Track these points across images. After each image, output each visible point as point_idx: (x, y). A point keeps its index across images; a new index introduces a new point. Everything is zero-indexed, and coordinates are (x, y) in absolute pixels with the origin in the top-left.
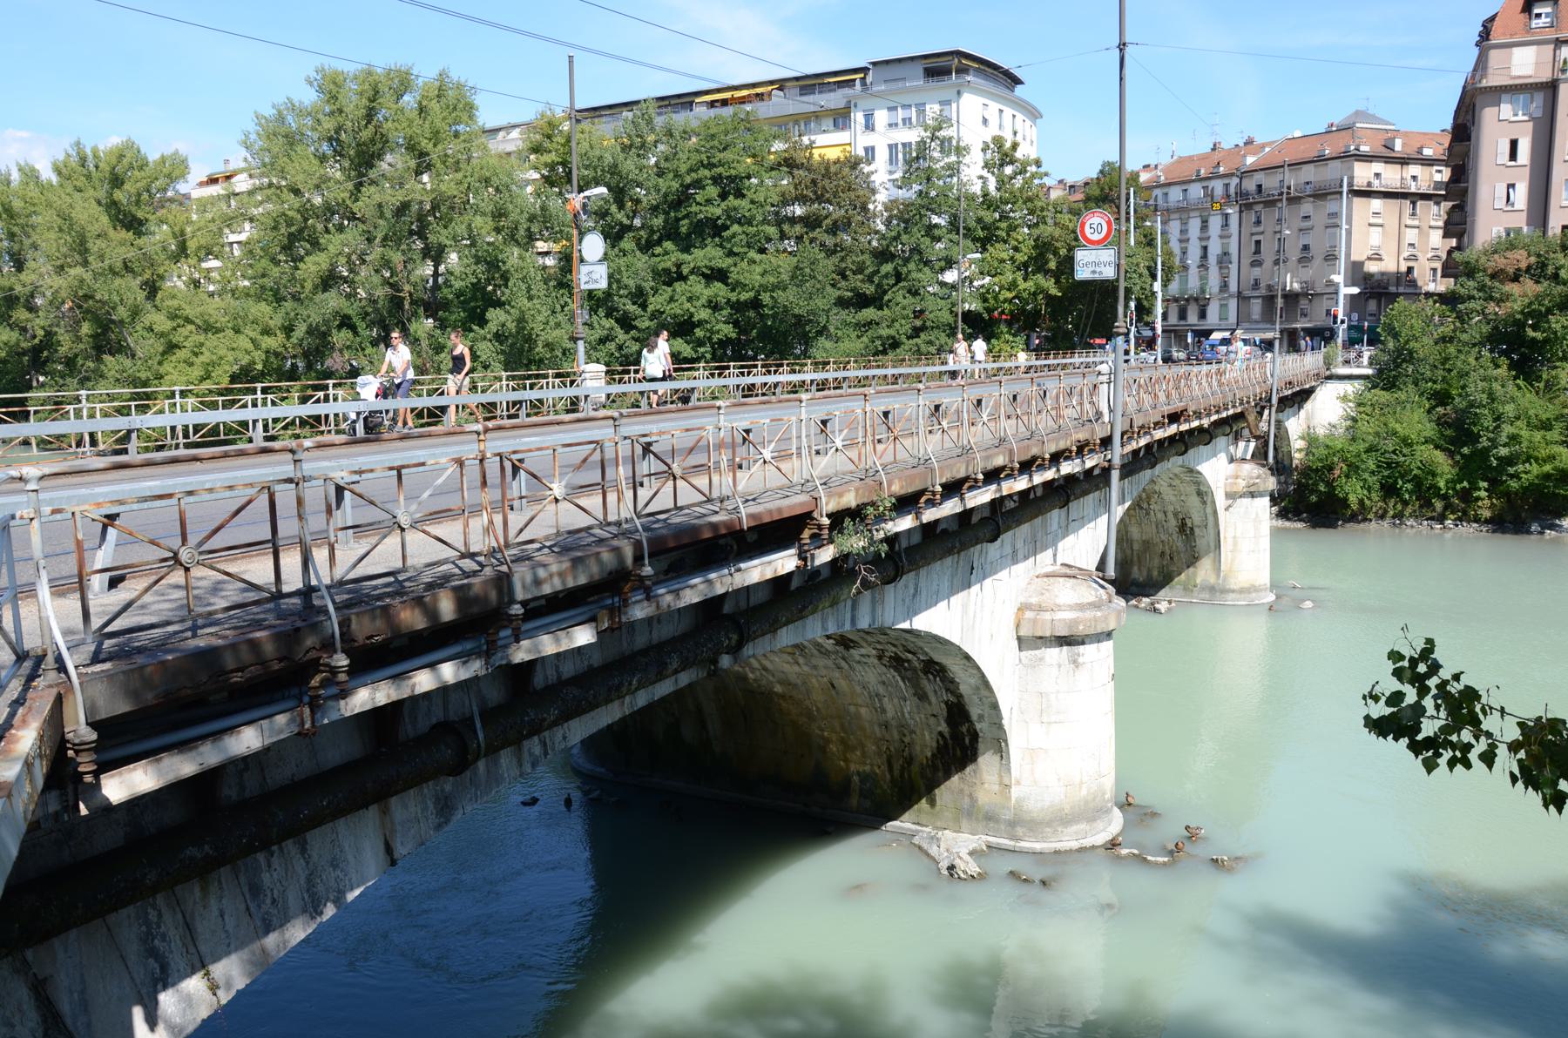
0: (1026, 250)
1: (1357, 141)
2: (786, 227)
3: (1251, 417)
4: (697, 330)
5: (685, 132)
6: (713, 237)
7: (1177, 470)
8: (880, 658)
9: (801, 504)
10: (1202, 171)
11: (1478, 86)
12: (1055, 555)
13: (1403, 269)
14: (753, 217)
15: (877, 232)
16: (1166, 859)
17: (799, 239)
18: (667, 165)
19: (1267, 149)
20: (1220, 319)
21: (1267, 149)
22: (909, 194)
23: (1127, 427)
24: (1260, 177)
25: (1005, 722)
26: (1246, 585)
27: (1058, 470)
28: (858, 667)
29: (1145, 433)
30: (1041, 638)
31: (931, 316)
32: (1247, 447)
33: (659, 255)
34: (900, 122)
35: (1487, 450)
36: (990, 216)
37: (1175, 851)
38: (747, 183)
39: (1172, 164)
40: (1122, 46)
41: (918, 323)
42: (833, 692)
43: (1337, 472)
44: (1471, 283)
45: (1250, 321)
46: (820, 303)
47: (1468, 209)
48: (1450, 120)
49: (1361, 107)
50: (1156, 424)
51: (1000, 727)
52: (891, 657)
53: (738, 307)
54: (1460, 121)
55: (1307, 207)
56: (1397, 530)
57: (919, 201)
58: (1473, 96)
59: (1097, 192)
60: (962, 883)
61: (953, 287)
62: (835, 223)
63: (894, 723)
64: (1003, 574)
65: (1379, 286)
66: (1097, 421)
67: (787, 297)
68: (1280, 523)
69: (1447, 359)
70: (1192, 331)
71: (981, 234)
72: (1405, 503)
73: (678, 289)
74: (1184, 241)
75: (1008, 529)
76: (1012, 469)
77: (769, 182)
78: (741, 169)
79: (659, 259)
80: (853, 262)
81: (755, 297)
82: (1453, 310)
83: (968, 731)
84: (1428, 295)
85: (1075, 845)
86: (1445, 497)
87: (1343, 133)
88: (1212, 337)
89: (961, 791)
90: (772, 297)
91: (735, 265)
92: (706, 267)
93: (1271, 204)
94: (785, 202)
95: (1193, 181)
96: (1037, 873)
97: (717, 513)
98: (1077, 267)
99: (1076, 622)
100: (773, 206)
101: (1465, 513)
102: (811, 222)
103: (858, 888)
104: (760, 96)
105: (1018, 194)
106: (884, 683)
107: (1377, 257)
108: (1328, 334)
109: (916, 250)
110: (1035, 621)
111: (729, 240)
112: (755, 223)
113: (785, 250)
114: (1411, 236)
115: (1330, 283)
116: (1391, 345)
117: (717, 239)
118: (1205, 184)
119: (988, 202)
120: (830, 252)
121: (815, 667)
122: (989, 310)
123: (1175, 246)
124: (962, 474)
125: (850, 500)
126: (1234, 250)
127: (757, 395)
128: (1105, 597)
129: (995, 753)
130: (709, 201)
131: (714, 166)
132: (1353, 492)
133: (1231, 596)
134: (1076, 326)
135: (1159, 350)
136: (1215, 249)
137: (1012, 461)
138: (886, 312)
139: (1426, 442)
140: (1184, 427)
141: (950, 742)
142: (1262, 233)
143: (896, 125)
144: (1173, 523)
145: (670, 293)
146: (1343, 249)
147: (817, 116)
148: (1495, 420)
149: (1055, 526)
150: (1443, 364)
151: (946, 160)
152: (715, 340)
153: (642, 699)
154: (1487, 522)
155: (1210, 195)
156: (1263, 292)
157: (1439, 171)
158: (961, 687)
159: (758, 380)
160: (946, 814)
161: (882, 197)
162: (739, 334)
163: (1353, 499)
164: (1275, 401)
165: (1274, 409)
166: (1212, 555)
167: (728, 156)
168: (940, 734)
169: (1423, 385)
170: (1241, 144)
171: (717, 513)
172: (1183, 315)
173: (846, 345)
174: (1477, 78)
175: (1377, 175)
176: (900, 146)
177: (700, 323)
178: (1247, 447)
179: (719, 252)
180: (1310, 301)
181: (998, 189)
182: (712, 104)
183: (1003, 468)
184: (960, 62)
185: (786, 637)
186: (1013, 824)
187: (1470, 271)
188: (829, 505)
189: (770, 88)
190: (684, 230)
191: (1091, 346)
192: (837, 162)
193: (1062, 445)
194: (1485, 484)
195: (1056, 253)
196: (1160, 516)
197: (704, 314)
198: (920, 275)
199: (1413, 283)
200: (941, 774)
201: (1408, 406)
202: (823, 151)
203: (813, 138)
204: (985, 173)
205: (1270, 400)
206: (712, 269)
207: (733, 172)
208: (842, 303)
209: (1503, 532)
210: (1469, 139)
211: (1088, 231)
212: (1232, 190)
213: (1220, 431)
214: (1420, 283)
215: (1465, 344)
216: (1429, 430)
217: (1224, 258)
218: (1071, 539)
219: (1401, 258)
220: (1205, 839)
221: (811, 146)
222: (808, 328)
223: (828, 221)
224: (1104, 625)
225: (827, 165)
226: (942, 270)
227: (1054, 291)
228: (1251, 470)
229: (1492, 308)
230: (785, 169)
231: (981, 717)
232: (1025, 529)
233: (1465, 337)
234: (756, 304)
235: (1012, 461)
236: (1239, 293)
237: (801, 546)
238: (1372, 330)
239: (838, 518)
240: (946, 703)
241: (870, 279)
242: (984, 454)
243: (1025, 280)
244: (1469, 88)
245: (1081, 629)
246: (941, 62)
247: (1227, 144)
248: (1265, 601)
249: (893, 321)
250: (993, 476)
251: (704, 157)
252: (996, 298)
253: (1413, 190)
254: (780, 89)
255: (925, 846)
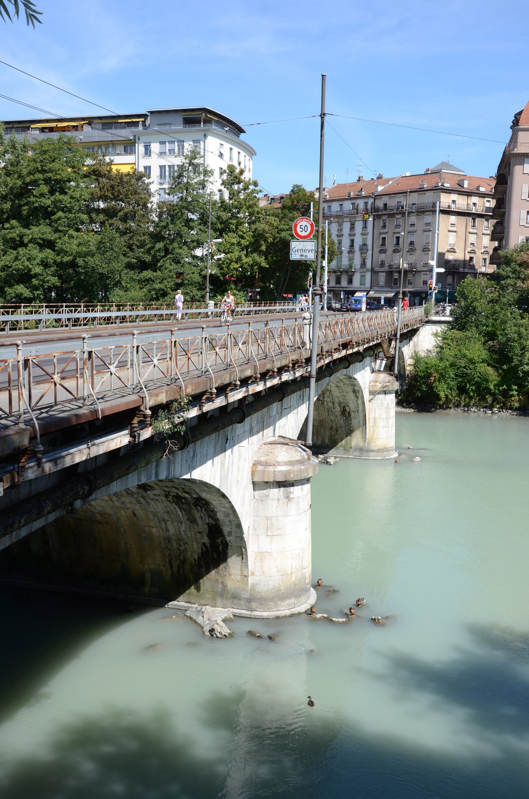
0: (248, 238)
1: (443, 180)
2: (94, 215)
3: (385, 346)
4: (34, 280)
5: (24, 147)
6: (45, 219)
7: (342, 377)
8: (167, 496)
9: (134, 401)
10: (352, 194)
11: (512, 152)
12: (274, 430)
13: (467, 258)
14: (72, 208)
15: (153, 222)
16: (344, 620)
17: (102, 224)
18: (13, 169)
19: (390, 183)
20: (361, 284)
21: (390, 183)
22: (174, 199)
23: (320, 352)
24: (385, 199)
25: (245, 536)
26: (381, 447)
27: (281, 378)
28: (152, 503)
29: (329, 355)
30: (267, 482)
31: (187, 277)
32: (381, 364)
33: (7, 229)
34: (167, 151)
35: (517, 366)
36: (225, 216)
37: (349, 615)
38: (68, 184)
39: (334, 188)
40: (323, 115)
41: (179, 281)
42: (135, 519)
43: (432, 379)
44: (508, 269)
45: (378, 286)
46: (116, 266)
47: (505, 224)
48: (496, 171)
49: (445, 160)
50: (335, 349)
51: (242, 539)
52: (174, 496)
53: (61, 265)
54: (501, 172)
55: (413, 219)
56: (466, 414)
57: (181, 203)
58: (509, 158)
59: (289, 203)
60: (219, 640)
61: (201, 259)
62: (126, 214)
63: (174, 538)
64: (245, 443)
65: (454, 268)
66: (303, 347)
67: (94, 261)
68: (400, 409)
69: (494, 313)
70: (344, 291)
71: (219, 226)
72: (471, 398)
73: (21, 252)
74: (340, 236)
75: (250, 414)
76: (256, 378)
77: (82, 185)
78: (64, 175)
79: (7, 231)
80: (138, 240)
81: (74, 260)
82: (498, 284)
83: (222, 542)
84: (484, 274)
85: (288, 612)
86: (493, 395)
87: (435, 175)
88: (356, 295)
89: (217, 580)
90: (84, 260)
91: (60, 238)
92: (40, 238)
93: (391, 216)
94: (93, 199)
95: (346, 199)
96: (265, 632)
97: (80, 407)
98: (292, 252)
99: (288, 472)
100: (85, 201)
101: (504, 404)
102: (110, 213)
103: (152, 647)
104: (75, 128)
105: (243, 202)
106: (168, 512)
107: (452, 251)
108: (424, 295)
109: (179, 234)
110: (263, 472)
111: (56, 221)
112: (73, 211)
113: (93, 231)
114: (472, 238)
115: (426, 264)
116: (463, 304)
117: (47, 221)
118: (353, 201)
119: (224, 206)
120: (123, 234)
121: (123, 503)
122: (224, 275)
123: (335, 238)
124: (227, 381)
125: (163, 398)
126: (369, 243)
127: (80, 325)
128: (306, 457)
129: (238, 556)
130: (42, 195)
131: (46, 171)
132: (442, 390)
133: (372, 454)
134: (277, 286)
135: (326, 302)
136: (358, 241)
137: (256, 373)
138: (159, 273)
139: (483, 362)
140: (350, 352)
141: (210, 549)
142: (386, 233)
143: (165, 153)
144: (338, 409)
145: (15, 255)
146: (436, 245)
147: (113, 144)
148: (522, 350)
149: (274, 412)
150: (492, 316)
151: (198, 179)
152: (46, 287)
153: (24, 532)
154: (516, 409)
155: (356, 208)
156: (386, 269)
157: (488, 201)
158: (218, 514)
159: (82, 315)
160: (207, 595)
161: (155, 199)
162: (62, 283)
163: (442, 394)
164: (398, 336)
165: (398, 341)
166: (361, 429)
167: (55, 165)
168: (204, 544)
169: (481, 327)
170: (375, 179)
171: (80, 407)
172: (338, 281)
173: (132, 294)
174: (512, 147)
175: (454, 201)
176: (167, 169)
177: (36, 276)
178: (381, 364)
179: (48, 229)
180: (414, 275)
181: (230, 199)
182: (43, 130)
183: (249, 378)
184: (206, 116)
185: (116, 487)
186: (249, 600)
187: (508, 261)
188: (150, 402)
189: (82, 122)
190: (25, 213)
191: (285, 299)
192: (128, 174)
193: (284, 363)
194: (516, 387)
195: (265, 240)
196: (330, 405)
197: (38, 270)
198: (181, 251)
199: (473, 267)
200: (203, 570)
201: (472, 340)
202: (119, 167)
203: (112, 158)
204: (222, 188)
205: (395, 335)
206: (44, 240)
207: (58, 177)
208: (129, 266)
209: (525, 416)
210: (506, 183)
211: (299, 230)
212: (369, 206)
213: (367, 354)
214: (476, 267)
215: (504, 304)
216: (484, 354)
217: (364, 248)
218: (283, 421)
219: (466, 252)
220: (366, 606)
221: (111, 163)
222: (108, 282)
223: (121, 213)
224: (306, 474)
225: (121, 176)
226: (195, 248)
227: (264, 264)
228: (384, 377)
229: (519, 283)
230: (94, 177)
231: (230, 533)
232: (259, 414)
233: (504, 300)
234: (73, 264)
235: (256, 373)
236: (372, 269)
237: (132, 428)
238: (451, 294)
239: (155, 409)
240: (208, 524)
241: (148, 252)
242: (240, 368)
243: (246, 256)
244: (507, 153)
245: (292, 477)
246: (195, 115)
247: (367, 178)
248: (392, 457)
249: (163, 280)
250: (245, 382)
251: (38, 165)
252: (228, 267)
253: (474, 211)
254: (89, 124)
255: (194, 617)
